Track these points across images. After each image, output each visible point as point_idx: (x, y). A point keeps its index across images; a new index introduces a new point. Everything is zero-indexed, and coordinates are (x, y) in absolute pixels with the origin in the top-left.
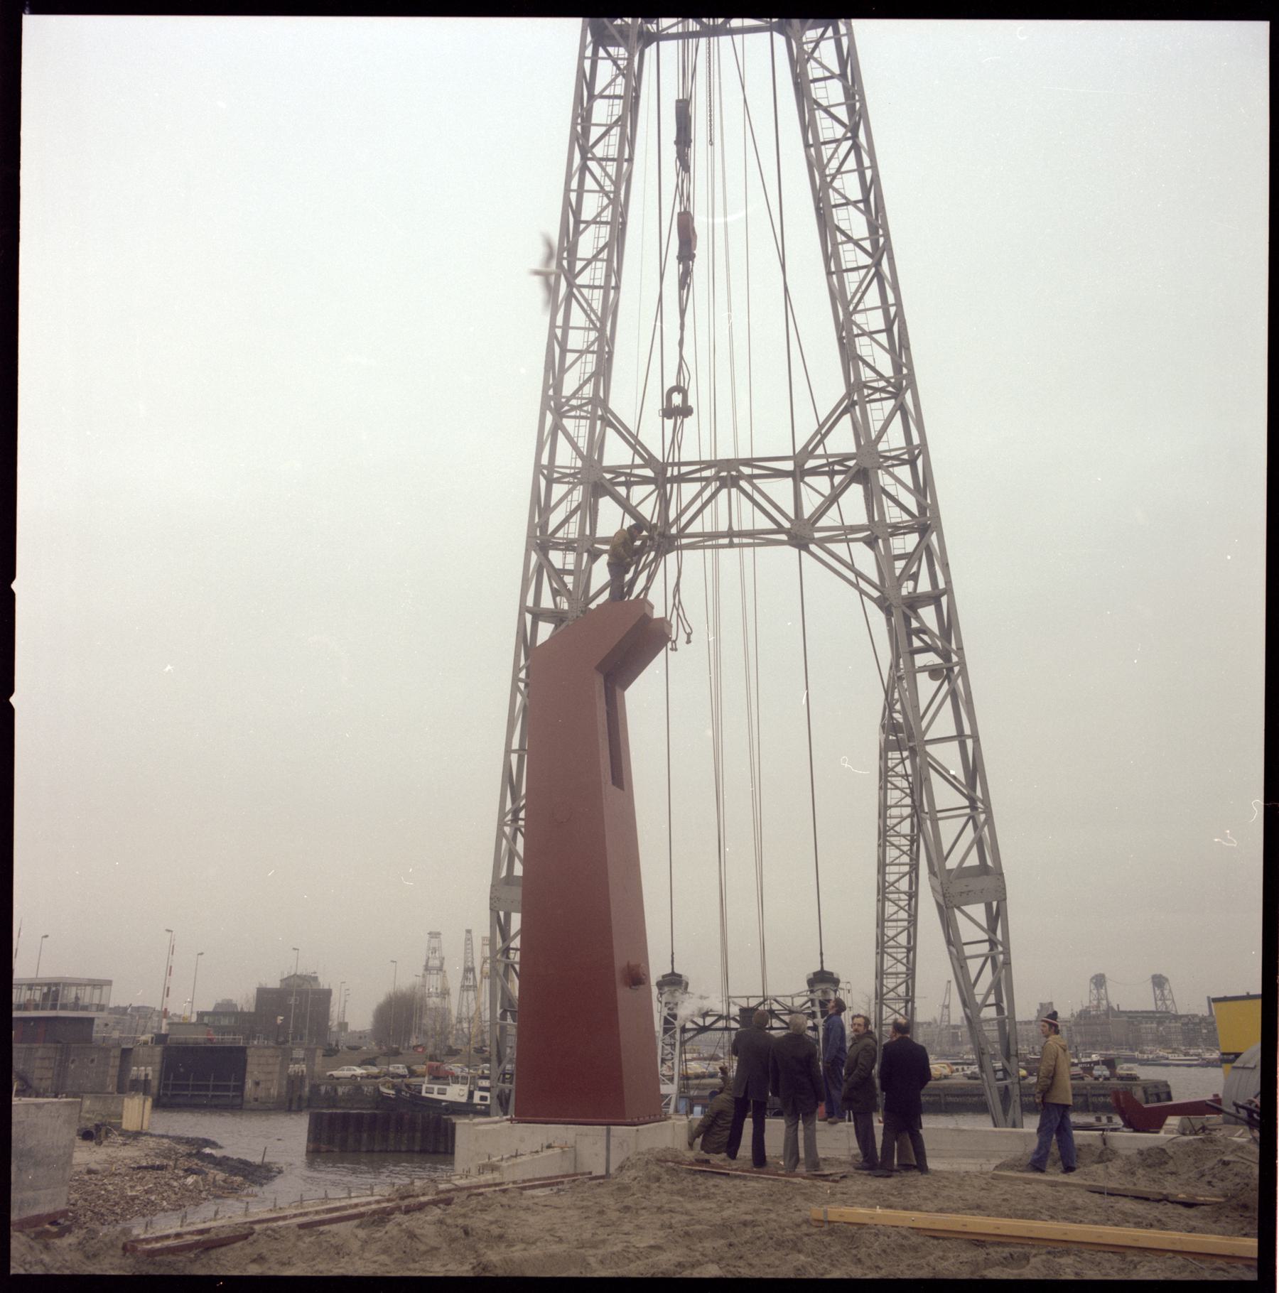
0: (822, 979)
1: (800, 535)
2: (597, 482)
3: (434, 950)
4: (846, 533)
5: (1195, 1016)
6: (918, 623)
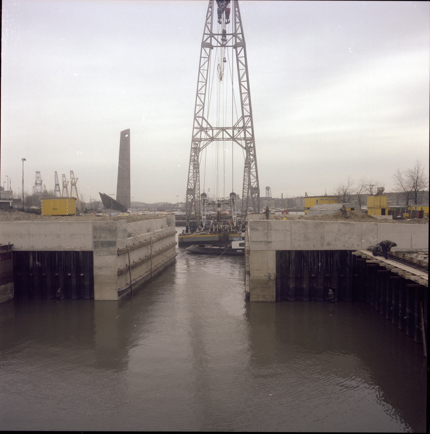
0: (233, 194)
1: (233, 138)
2: (202, 129)
3: (38, 178)
4: (240, 139)
5: (278, 199)
6: (250, 148)
